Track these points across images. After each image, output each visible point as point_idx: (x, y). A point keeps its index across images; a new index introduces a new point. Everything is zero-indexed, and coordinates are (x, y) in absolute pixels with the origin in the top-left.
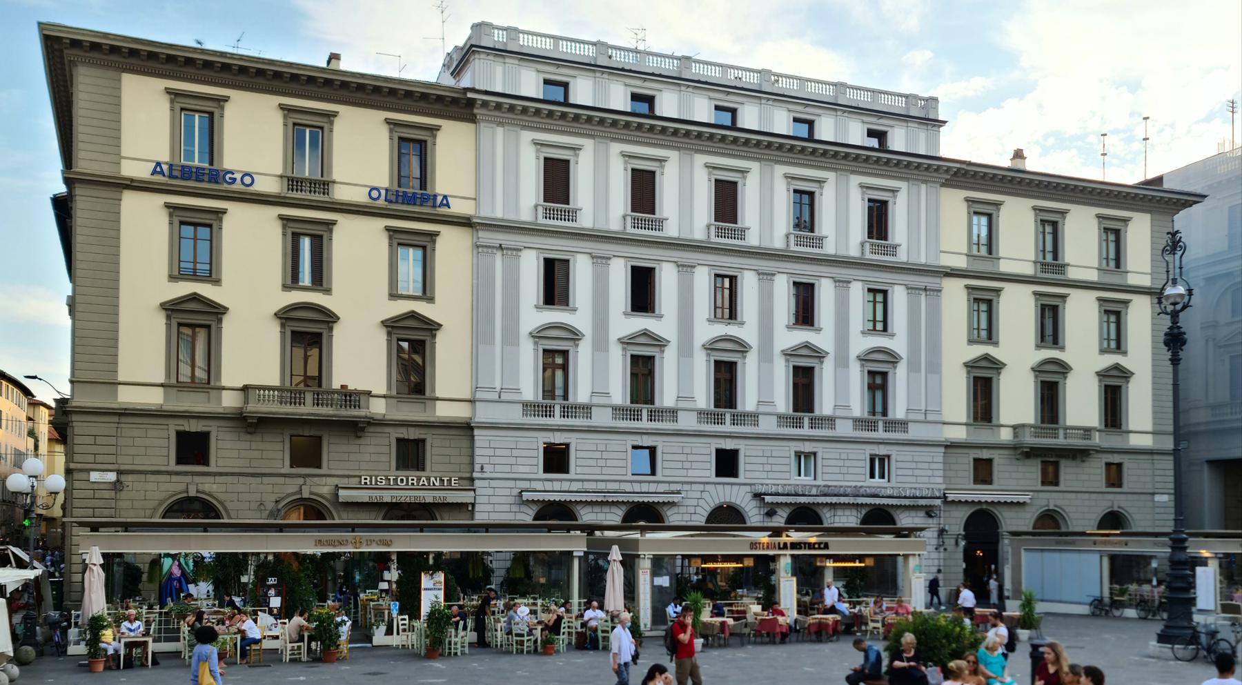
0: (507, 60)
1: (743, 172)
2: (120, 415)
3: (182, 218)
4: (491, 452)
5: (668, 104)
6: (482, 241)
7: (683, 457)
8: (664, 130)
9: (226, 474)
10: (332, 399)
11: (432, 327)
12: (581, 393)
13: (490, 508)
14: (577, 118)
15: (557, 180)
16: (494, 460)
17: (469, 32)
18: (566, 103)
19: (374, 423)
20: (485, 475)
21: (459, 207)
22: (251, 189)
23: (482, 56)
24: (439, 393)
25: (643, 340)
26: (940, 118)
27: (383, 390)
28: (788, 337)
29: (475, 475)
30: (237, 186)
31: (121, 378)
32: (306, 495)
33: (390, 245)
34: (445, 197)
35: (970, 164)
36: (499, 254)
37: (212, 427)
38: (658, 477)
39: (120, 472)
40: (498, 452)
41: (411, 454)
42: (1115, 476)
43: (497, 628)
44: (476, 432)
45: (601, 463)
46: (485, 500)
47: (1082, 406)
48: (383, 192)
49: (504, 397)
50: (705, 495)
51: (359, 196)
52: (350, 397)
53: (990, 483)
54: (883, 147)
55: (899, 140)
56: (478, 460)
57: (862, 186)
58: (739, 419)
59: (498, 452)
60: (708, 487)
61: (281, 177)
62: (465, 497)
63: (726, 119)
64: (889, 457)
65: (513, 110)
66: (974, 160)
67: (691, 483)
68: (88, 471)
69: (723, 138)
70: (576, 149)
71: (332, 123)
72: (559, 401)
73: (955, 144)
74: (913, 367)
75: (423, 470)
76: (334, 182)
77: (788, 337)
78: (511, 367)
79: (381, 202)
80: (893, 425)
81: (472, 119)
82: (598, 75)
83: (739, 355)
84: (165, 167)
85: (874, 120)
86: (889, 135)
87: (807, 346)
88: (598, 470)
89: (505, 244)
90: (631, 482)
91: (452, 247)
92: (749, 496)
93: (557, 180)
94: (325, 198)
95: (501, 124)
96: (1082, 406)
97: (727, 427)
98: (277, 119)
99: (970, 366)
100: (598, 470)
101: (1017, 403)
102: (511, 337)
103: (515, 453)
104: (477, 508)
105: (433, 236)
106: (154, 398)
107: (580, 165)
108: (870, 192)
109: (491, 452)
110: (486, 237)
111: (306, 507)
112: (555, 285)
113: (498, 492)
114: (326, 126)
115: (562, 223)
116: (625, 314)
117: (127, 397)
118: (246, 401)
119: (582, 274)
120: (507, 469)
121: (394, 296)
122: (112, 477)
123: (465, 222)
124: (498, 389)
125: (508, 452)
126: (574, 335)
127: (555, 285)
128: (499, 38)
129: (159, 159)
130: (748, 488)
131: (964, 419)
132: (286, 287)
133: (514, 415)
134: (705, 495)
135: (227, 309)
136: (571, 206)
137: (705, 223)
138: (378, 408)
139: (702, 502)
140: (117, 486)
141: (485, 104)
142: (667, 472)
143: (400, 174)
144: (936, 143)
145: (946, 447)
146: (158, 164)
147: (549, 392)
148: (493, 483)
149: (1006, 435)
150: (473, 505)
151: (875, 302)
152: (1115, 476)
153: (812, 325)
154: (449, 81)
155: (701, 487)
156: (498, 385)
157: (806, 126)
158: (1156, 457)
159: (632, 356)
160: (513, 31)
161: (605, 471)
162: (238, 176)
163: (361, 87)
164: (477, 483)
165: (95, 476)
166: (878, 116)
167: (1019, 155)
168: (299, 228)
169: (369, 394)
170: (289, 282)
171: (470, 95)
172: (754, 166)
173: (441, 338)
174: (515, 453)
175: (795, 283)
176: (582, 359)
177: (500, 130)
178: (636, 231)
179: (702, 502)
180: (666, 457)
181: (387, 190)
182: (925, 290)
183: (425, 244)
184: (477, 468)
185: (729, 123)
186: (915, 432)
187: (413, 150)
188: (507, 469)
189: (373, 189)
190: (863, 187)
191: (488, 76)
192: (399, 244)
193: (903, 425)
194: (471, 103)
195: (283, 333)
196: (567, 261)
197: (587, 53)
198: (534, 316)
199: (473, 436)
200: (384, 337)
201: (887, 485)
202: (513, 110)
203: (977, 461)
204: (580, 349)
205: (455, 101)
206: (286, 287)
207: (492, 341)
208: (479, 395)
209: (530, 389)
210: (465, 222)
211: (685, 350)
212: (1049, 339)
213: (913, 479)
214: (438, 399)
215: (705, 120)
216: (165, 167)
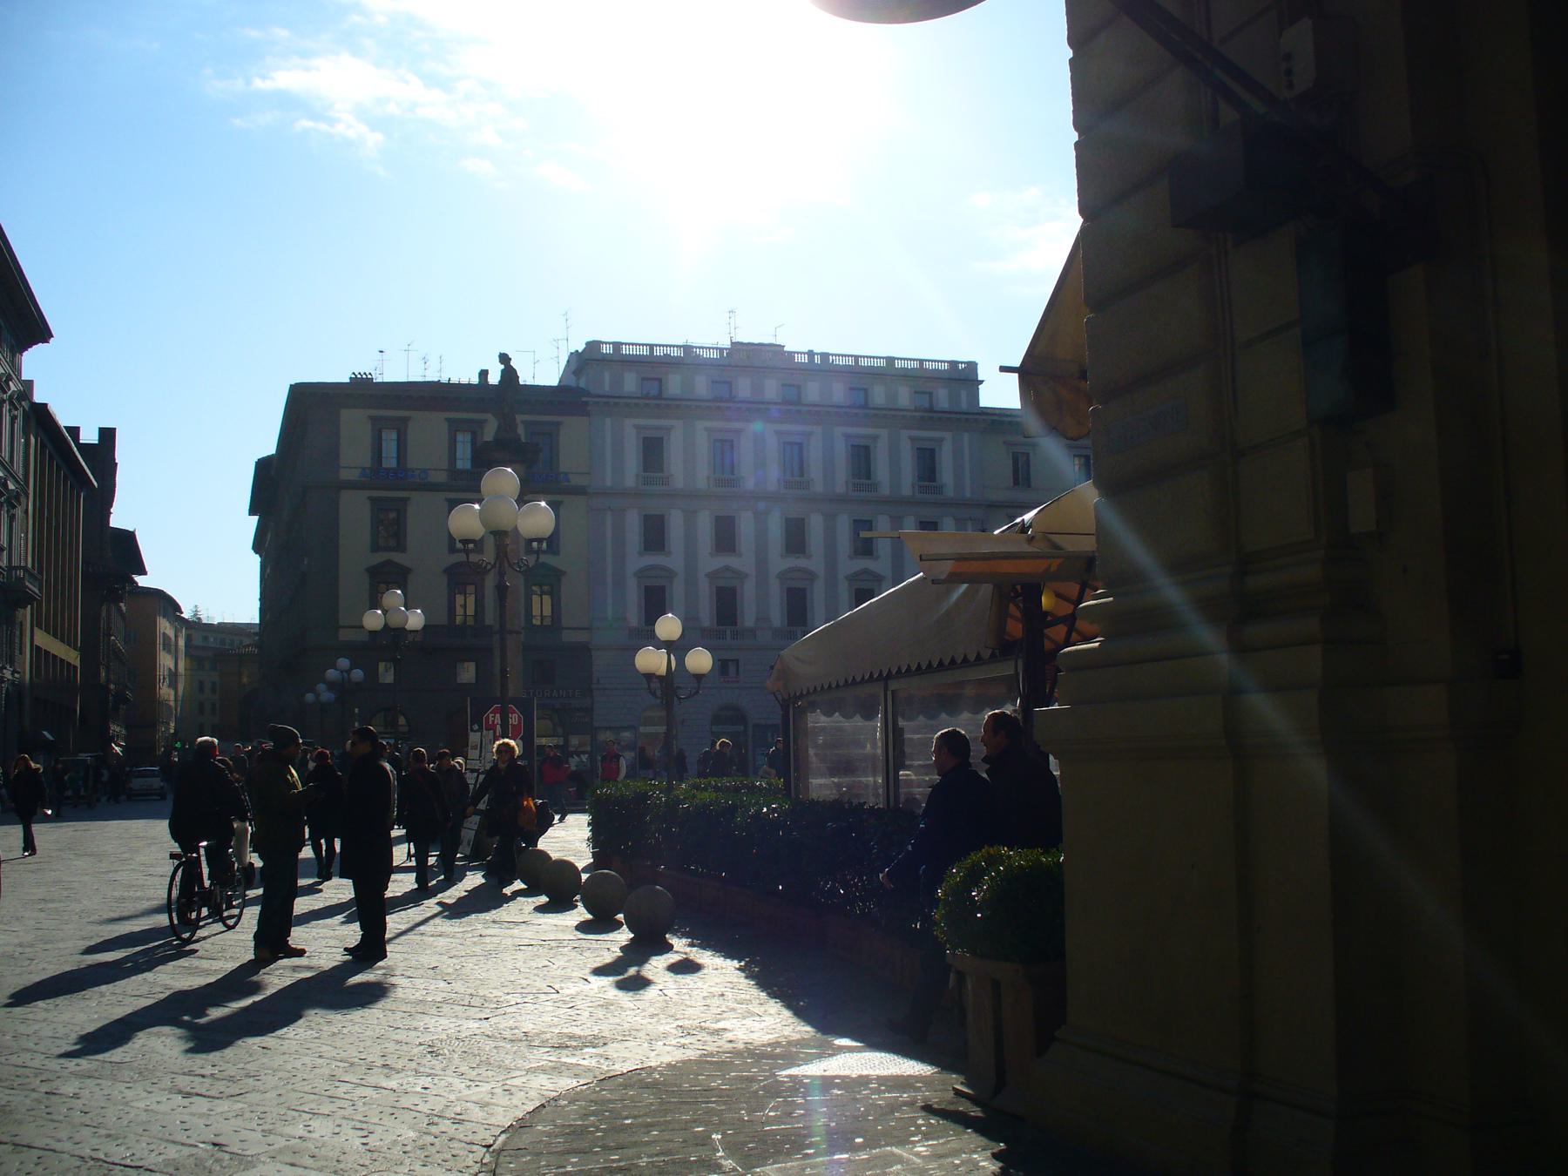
21: (576, 481)
55: (943, 399)
126: (670, 574)
198: (636, 561)
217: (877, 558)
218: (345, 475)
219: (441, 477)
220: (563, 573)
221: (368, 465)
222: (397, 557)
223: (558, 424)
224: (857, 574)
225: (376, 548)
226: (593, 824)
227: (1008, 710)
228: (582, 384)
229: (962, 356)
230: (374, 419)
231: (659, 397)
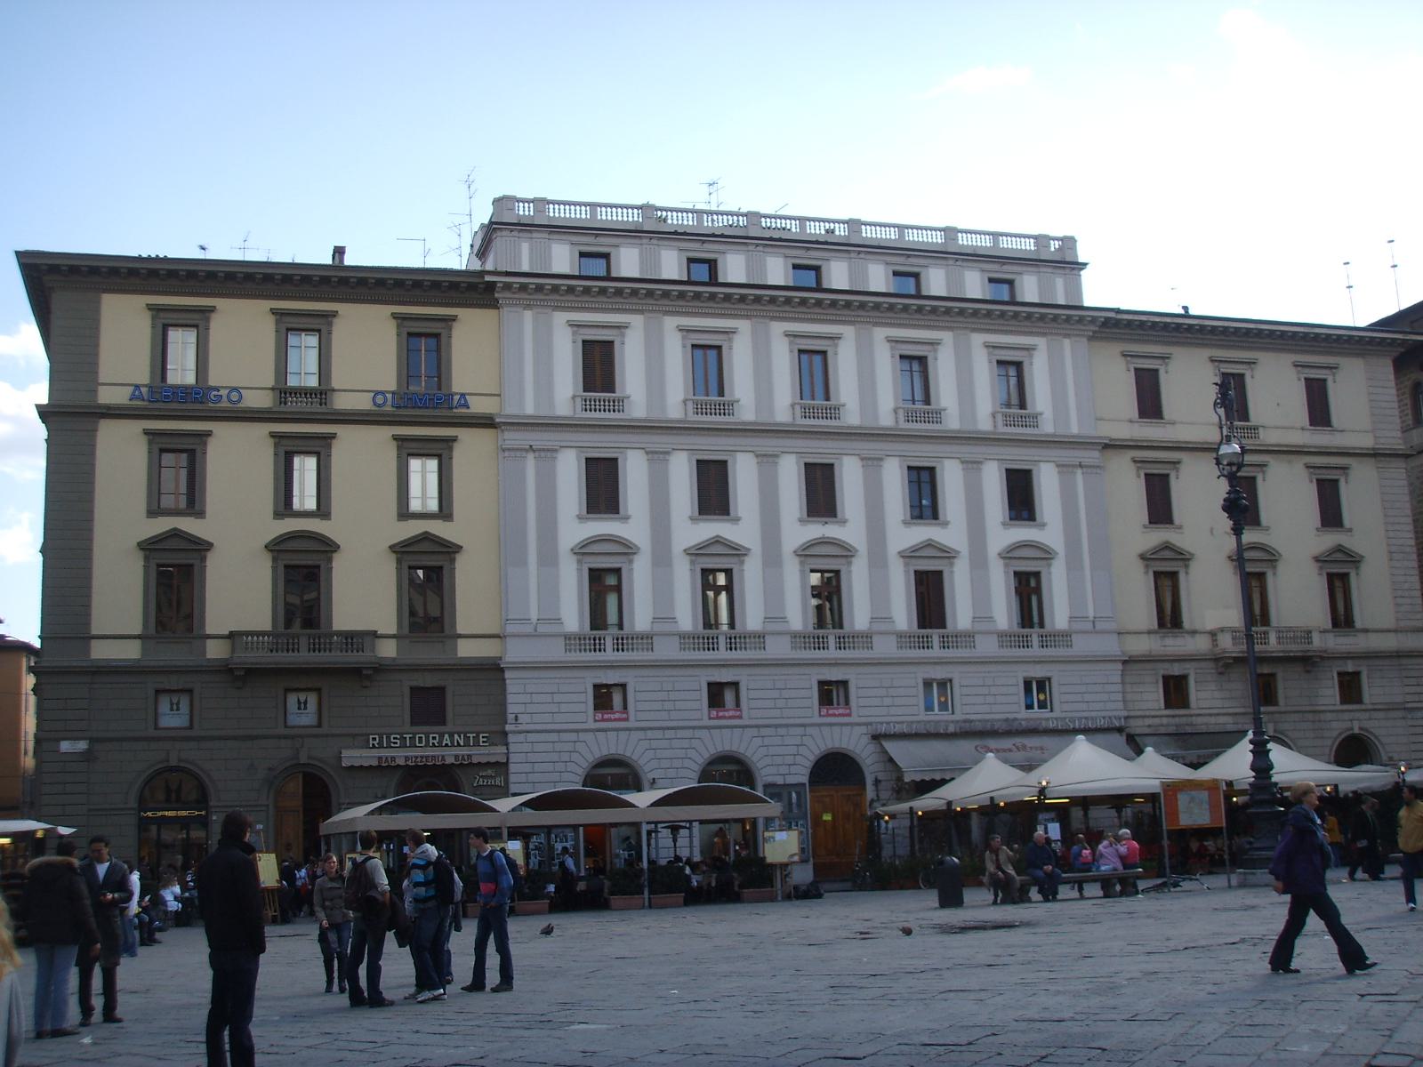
0: (1042, 269)
1: (621, 327)
2: (94, 673)
3: (161, 444)
4: (527, 698)
5: (838, 275)
6: (508, 444)
7: (775, 694)
8: (934, 310)
9: (212, 738)
10: (331, 643)
11: (450, 550)
12: (641, 617)
13: (527, 768)
14: (834, 303)
15: (598, 366)
16: (530, 708)
17: (490, 210)
18: (919, 296)
19: (381, 669)
20: (521, 728)
21: (478, 406)
22: (240, 405)
23: (504, 233)
24: (460, 630)
25: (1167, 554)
26: (1080, 260)
27: (393, 630)
28: (904, 535)
29: (508, 728)
30: (225, 404)
31: (94, 632)
32: (303, 760)
33: (399, 456)
34: (463, 395)
35: (1118, 311)
36: (1079, 471)
37: (1190, 670)
38: (325, 730)
39: (92, 740)
40: (536, 698)
41: (429, 707)
42: (1350, 688)
43: (1086, 893)
44: (508, 675)
45: (888, 701)
46: (521, 758)
47: (1298, 600)
48: (389, 396)
49: (1099, 626)
50: (580, 746)
51: (363, 403)
52: (354, 639)
53: (1276, 704)
54: (713, 280)
55: (1030, 288)
56: (511, 709)
57: (890, 340)
58: (1049, 639)
59: (536, 698)
60: (809, 730)
61: (273, 389)
62: (495, 753)
63: (808, 279)
64: (1049, 679)
65: (542, 290)
66: (1123, 307)
67: (787, 726)
68: (58, 740)
69: (1003, 314)
70: (1029, 349)
71: (330, 324)
72: (614, 631)
73: (1098, 291)
74: (1074, 563)
75: (443, 723)
76: (334, 390)
77: (904, 535)
78: (550, 591)
79: (388, 408)
80: (1049, 639)
81: (494, 305)
82: (1067, 271)
83: (843, 561)
84: (144, 390)
85: (995, 267)
86: (922, 276)
87: (929, 544)
88: (664, 715)
89: (536, 444)
90: (819, 725)
91: (471, 448)
92: (865, 739)
93: (598, 366)
94: (323, 409)
95: (1067, 336)
96: (1298, 600)
97: (832, 653)
98: (391, 328)
99: (149, 547)
100: (777, 713)
101: (1213, 603)
102: (549, 558)
103: (558, 698)
104: (512, 768)
105: (450, 442)
106: (131, 652)
107: (940, 362)
108: (997, 352)
109: (527, 698)
110: (513, 438)
111: (306, 775)
112: (603, 488)
113: (538, 747)
114: (324, 328)
115: (607, 415)
116: (580, 517)
117: (101, 652)
118: (233, 650)
119: (951, 479)
120: (548, 718)
121: (154, 511)
122: (82, 745)
123: (487, 422)
124: (1091, 619)
125: (548, 698)
126: (628, 550)
127: (603, 488)
128: (524, 211)
129: (138, 382)
130: (863, 729)
131: (137, 629)
132: (278, 515)
133: (555, 651)
134: (580, 746)
135: (211, 545)
136: (618, 394)
137: (570, 394)
138: (388, 650)
139: (802, 750)
140: (87, 756)
141: (508, 287)
142: (1066, 707)
143: (408, 370)
144: (1076, 289)
145: (1124, 662)
146: (137, 387)
147: (709, 622)
148: (531, 737)
149: (1201, 645)
150: (506, 764)
151: (919, 482)
152: (1350, 688)
153: (728, 513)
154: (476, 266)
155: (800, 730)
156: (1091, 614)
157: (706, 266)
158: (1404, 661)
159: (591, 570)
160: (540, 203)
161: (674, 715)
162: (224, 392)
163: (230, 276)
164: (511, 738)
165: (65, 746)
166: (1001, 264)
167: (339, 252)
168: (290, 445)
169: (374, 635)
170: (281, 508)
171: (488, 278)
172: (1040, 342)
173: (462, 563)
174: (558, 698)
175: (910, 468)
176: (751, 577)
177: (1067, 342)
178: (589, 415)
179: (802, 750)
180: (753, 694)
181: (393, 393)
182: (1081, 466)
183: (441, 450)
184: (511, 717)
185: (603, 273)
186: (1081, 646)
187: (424, 345)
188: (548, 718)
189: (377, 393)
190: (893, 341)
191: (523, 256)
192: (409, 455)
193: (1064, 637)
194: (491, 287)
195: (274, 569)
196: (616, 460)
197: (633, 217)
198: (574, 528)
199: (504, 680)
200: (269, 564)
201: (1051, 715)
202: (542, 290)
203: (1167, 680)
204: (956, 569)
205: (472, 287)
206: (278, 515)
207: (523, 562)
208: (510, 629)
209: (573, 615)
210: (487, 422)
211: (979, 561)
212: (927, 512)
213: (1084, 706)
214: (461, 636)
215: (979, 296)
216: (144, 390)
217: (627, 518)
218: (107, 396)
219: (259, 400)
220: (458, 548)
221: (146, 381)
222: (188, 525)
223: (449, 320)
224: (916, 549)
225: (154, 511)
226: (1292, 897)
227: (203, 813)
228: (489, 267)
229: (1056, 228)
230: (155, 310)
231: (819, 288)
